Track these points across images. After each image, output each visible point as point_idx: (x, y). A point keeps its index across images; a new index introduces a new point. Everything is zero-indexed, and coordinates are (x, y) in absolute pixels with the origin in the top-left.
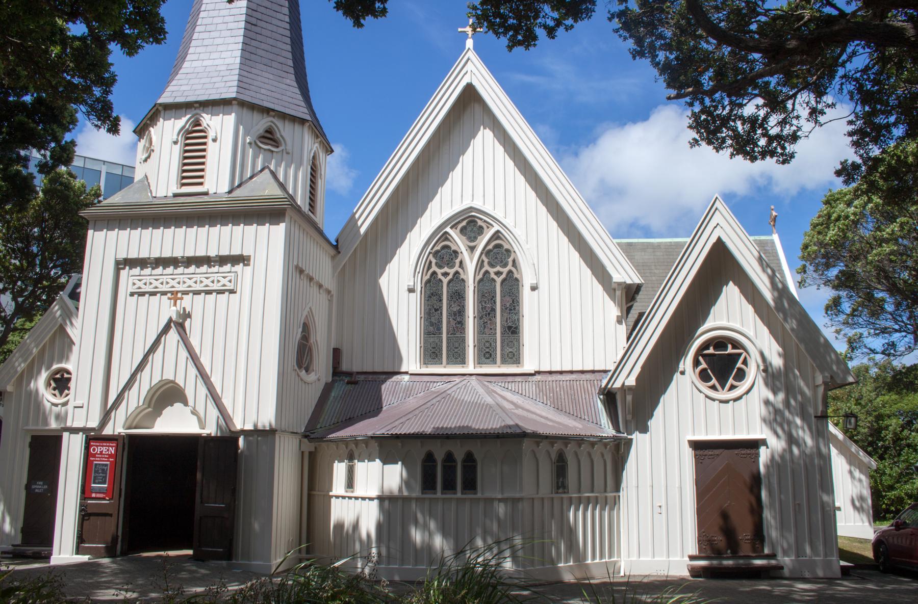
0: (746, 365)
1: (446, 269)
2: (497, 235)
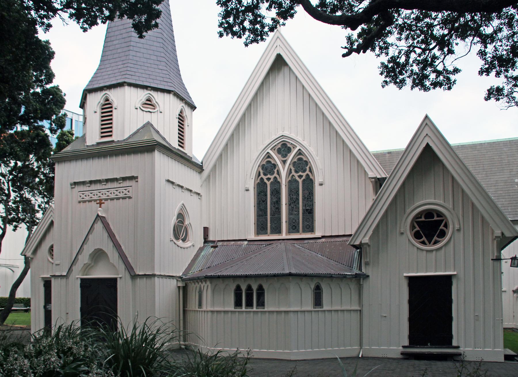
0: (446, 228)
1: (269, 176)
2: (300, 152)
